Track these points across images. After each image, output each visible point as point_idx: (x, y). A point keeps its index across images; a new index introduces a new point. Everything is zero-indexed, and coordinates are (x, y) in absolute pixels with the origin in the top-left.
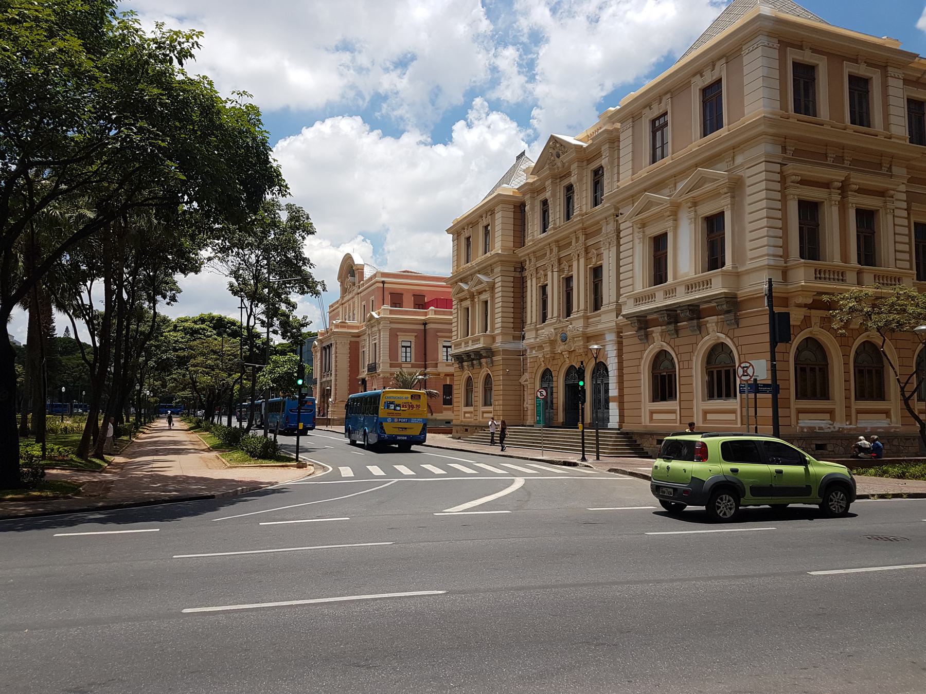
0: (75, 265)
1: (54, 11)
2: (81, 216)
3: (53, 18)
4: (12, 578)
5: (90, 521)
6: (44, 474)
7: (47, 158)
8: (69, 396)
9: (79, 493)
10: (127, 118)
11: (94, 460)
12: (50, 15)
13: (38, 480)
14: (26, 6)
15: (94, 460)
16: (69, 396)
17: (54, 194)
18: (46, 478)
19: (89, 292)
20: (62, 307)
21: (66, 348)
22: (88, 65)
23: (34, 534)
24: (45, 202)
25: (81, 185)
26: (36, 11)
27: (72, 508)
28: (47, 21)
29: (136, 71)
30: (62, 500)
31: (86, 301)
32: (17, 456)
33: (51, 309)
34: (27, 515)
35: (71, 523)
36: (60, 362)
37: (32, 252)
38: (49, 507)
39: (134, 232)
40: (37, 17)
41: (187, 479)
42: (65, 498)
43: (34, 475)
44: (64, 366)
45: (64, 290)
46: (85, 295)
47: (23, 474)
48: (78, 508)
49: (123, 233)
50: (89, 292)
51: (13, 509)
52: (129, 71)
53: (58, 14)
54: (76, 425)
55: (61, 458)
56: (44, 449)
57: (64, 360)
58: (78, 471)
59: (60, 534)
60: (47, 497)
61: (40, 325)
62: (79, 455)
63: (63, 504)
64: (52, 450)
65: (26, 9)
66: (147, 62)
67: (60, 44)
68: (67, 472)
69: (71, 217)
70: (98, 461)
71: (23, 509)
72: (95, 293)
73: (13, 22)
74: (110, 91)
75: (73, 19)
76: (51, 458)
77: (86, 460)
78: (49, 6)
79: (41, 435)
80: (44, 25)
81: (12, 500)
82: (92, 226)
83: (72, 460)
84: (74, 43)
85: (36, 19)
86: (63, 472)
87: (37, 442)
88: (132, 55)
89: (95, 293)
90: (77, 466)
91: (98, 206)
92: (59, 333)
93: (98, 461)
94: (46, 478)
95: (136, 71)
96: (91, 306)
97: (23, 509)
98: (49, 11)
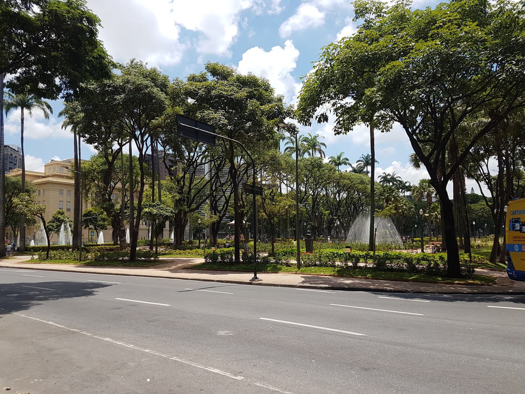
0: (477, 151)
1: (458, 12)
2: (480, 122)
3: (458, 17)
4: (471, 327)
5: (507, 300)
6: (474, 271)
7: (459, 95)
8: (477, 227)
9: (495, 283)
10: (508, 57)
11: (500, 264)
12: (456, 16)
13: (470, 274)
14: (443, 16)
15: (500, 264)
16: (477, 227)
17: (464, 113)
18: (475, 273)
19: (487, 166)
20: (470, 176)
21: (472, 199)
22: (480, 34)
23: (475, 304)
24: (461, 119)
25: (478, 105)
26: (449, 16)
27: (493, 291)
28: (455, 19)
29: (510, 25)
30: (486, 286)
31: (486, 171)
32: (459, 259)
33: (464, 178)
34: (469, 293)
35: (496, 300)
36: (470, 208)
37: (454, 150)
38: (480, 290)
39: (512, 125)
40: (450, 19)
41: (186, 272)
42: (487, 285)
43: (469, 271)
44: (472, 210)
45: (471, 167)
46: (484, 167)
47: (462, 270)
48: (497, 292)
49: (507, 125)
50: (487, 166)
51: (460, 289)
52: (506, 27)
53: (460, 13)
54: (484, 243)
55: (480, 262)
56: (470, 256)
57: (473, 206)
58: (492, 270)
59: (491, 306)
60: (478, 284)
61: (459, 187)
62: (492, 260)
63: (487, 288)
64: (475, 257)
65: (444, 18)
66: (517, 17)
67: (466, 29)
68: (485, 271)
69: (474, 124)
70: (502, 265)
71: (466, 290)
72: (492, 166)
73: (441, 27)
74: (496, 44)
75: (469, 12)
76: (475, 262)
77: (495, 264)
78: (456, 11)
79: (468, 248)
80: (455, 22)
81: (458, 284)
82: (488, 128)
83: (487, 263)
84: (471, 26)
85: (450, 21)
86: (483, 270)
87: (466, 252)
88: (507, 17)
89: (492, 166)
90: (491, 267)
91: (490, 114)
92: (468, 191)
93: (502, 265)
94: (475, 273)
95: (510, 25)
96: (489, 173)
97: (466, 290)
98: (456, 14)
